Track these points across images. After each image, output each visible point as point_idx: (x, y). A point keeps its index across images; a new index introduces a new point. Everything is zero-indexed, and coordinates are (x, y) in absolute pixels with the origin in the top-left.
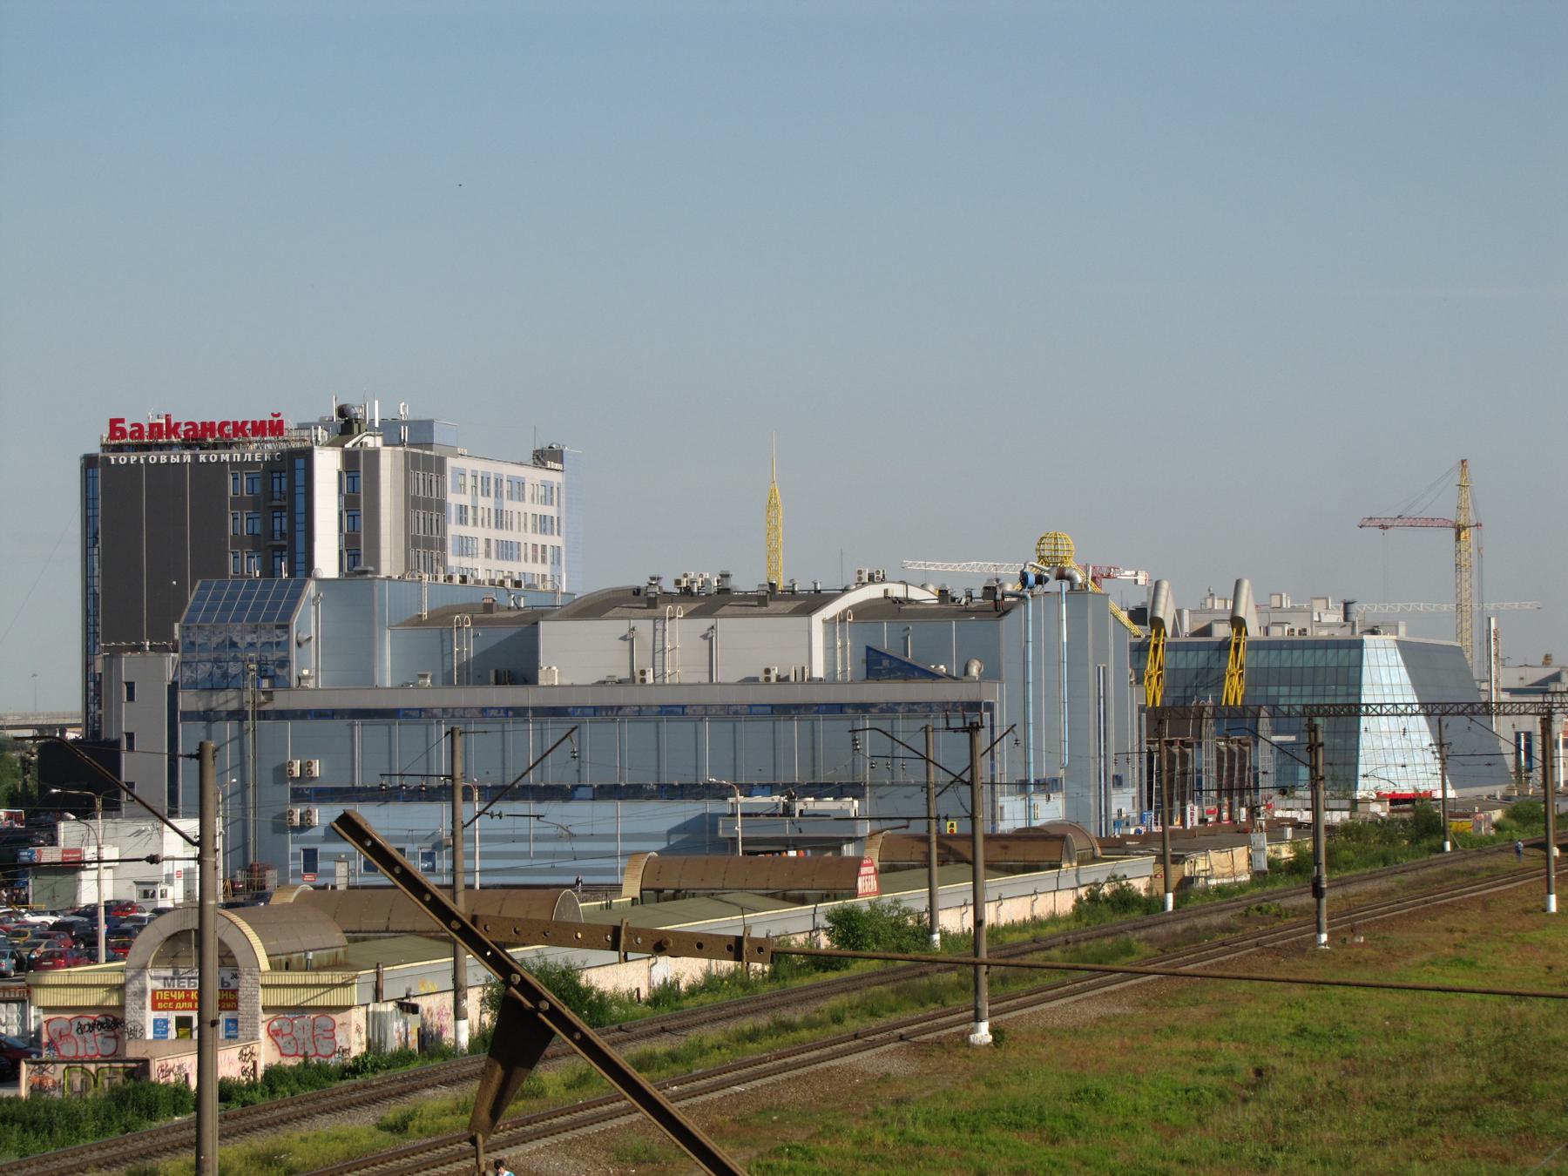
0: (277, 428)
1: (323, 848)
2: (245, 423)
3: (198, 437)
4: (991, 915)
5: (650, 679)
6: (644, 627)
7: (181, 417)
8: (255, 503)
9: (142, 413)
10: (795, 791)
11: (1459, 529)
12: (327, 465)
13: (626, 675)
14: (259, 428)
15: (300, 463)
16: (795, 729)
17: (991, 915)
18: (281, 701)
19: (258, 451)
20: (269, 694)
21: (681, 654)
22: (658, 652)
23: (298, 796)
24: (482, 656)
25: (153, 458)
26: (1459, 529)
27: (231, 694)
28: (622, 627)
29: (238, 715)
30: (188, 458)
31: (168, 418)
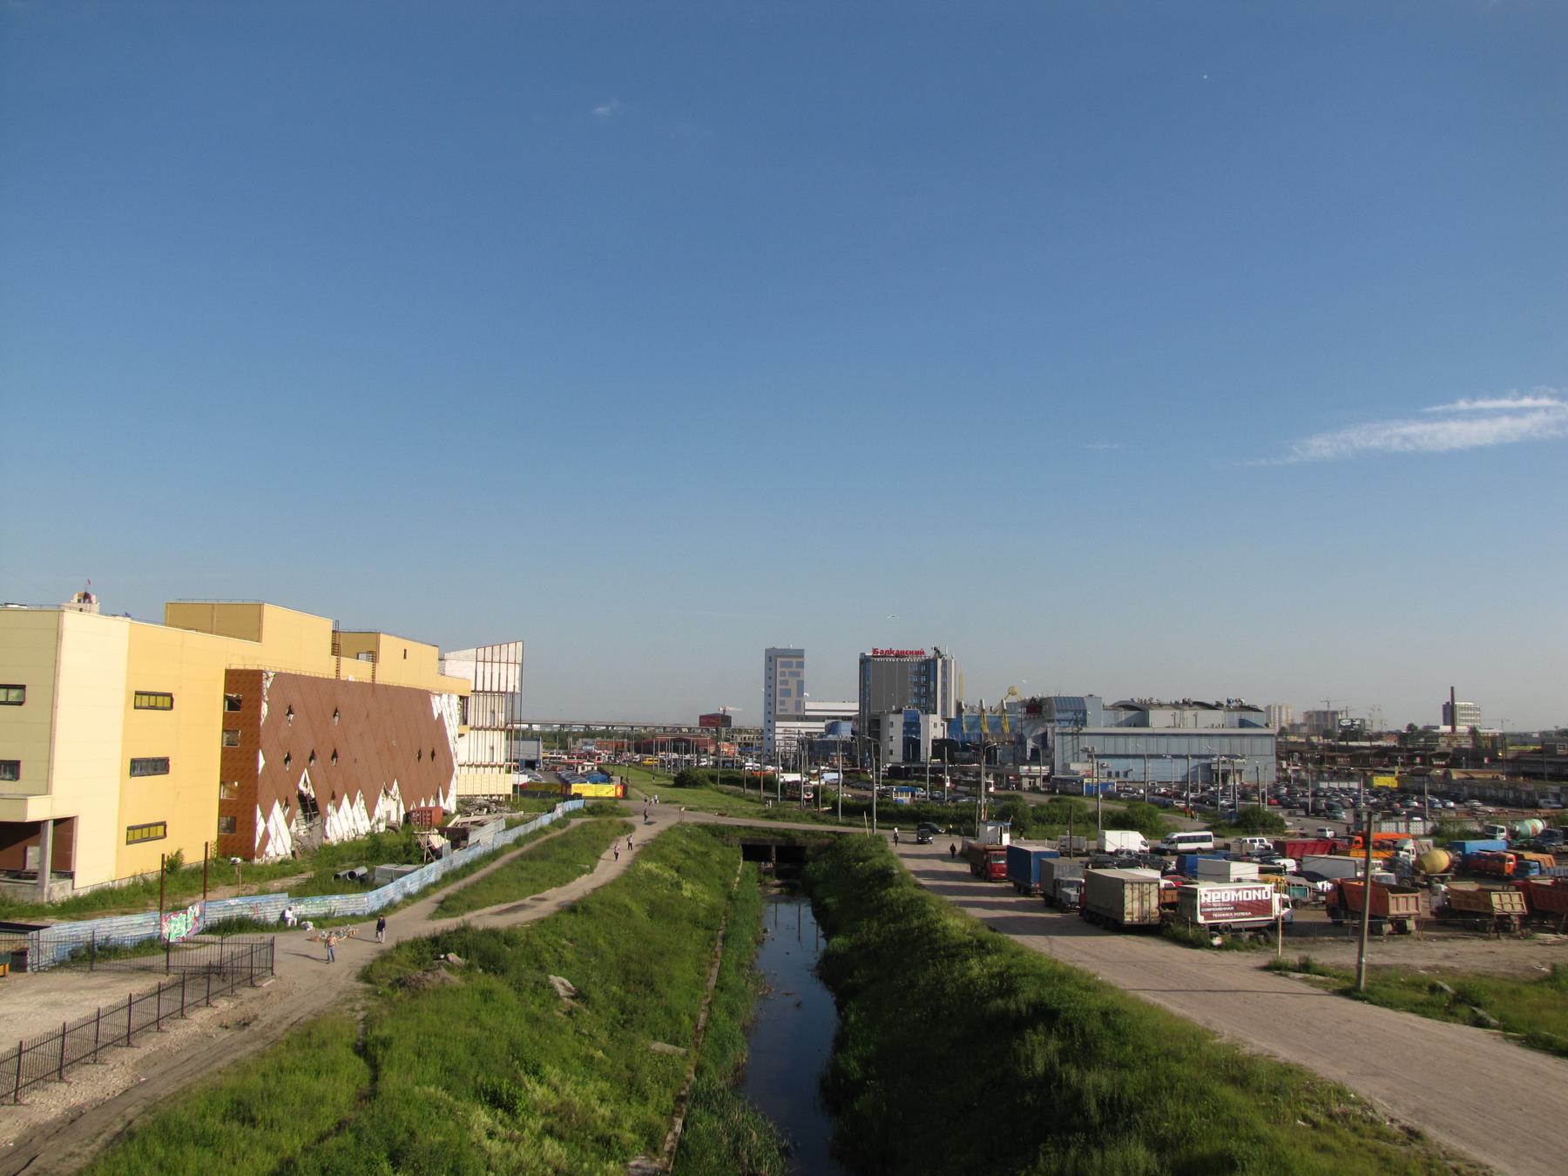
3: (900, 655)
7: (895, 649)
12: (940, 662)
18: (1085, 730)
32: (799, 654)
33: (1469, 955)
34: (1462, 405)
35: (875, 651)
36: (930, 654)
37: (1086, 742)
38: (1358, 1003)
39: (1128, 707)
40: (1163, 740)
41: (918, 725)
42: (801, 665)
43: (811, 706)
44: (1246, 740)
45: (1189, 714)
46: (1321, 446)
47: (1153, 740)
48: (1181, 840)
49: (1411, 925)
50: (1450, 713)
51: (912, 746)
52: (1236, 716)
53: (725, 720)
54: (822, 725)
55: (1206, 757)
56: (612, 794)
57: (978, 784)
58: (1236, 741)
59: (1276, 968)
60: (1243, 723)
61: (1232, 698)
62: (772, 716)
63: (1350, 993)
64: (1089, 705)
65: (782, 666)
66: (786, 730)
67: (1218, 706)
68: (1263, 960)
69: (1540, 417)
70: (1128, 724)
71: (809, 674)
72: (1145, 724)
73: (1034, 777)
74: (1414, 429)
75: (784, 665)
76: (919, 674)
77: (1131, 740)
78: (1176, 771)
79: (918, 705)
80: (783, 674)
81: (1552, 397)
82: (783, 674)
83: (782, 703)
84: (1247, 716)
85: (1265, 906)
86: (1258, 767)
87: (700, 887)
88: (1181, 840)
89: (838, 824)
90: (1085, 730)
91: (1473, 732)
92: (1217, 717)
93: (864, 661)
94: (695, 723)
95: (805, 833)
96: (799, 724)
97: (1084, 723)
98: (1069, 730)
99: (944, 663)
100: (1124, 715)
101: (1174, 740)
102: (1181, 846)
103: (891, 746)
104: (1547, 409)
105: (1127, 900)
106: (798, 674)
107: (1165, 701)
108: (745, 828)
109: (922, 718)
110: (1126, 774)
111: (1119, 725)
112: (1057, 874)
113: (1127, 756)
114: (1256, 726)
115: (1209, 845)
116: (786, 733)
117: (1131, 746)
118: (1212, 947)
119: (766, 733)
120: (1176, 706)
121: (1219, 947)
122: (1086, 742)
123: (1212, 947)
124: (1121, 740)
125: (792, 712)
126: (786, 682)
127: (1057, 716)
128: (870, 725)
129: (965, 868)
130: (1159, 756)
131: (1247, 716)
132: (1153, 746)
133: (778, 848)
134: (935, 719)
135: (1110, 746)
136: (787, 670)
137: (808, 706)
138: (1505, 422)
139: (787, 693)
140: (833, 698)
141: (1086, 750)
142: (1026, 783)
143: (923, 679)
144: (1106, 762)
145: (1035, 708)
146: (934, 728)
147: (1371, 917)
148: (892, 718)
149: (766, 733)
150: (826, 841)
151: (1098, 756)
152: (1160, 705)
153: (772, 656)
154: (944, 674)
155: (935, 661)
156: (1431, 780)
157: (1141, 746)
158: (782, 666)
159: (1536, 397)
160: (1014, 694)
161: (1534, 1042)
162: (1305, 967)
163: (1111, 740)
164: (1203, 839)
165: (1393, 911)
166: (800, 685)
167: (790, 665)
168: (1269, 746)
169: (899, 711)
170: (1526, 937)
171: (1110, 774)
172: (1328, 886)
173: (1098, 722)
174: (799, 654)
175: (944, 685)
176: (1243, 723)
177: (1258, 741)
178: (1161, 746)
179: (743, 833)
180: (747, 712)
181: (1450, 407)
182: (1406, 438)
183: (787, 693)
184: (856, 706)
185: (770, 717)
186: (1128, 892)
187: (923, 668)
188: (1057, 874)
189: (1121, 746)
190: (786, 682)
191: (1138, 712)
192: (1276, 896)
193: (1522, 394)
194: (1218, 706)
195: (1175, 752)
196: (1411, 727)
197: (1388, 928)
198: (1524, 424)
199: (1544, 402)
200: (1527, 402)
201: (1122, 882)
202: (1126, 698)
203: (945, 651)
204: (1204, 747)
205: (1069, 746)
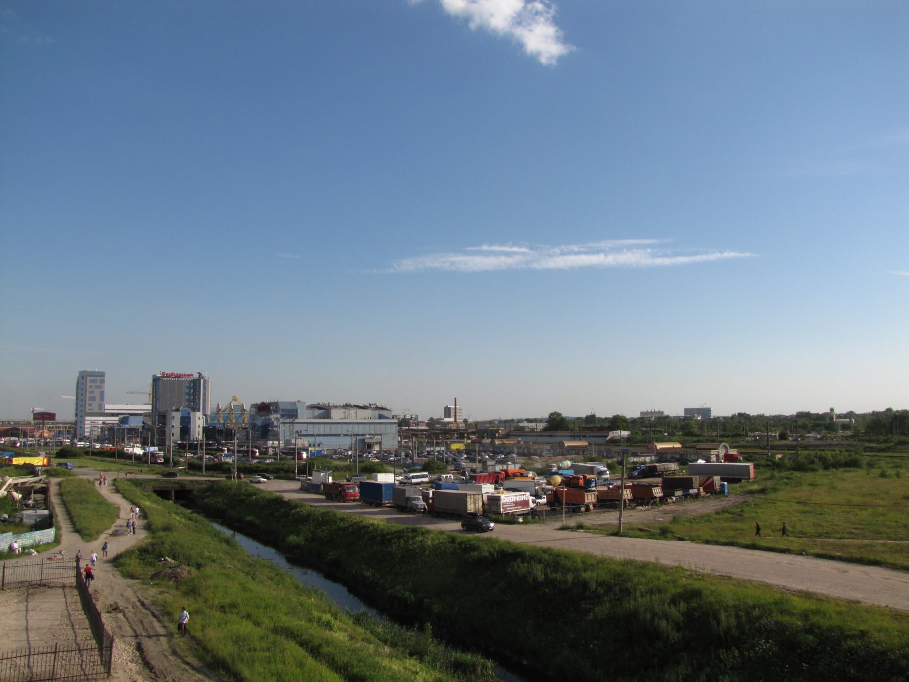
7: (175, 373)
12: (202, 381)
16: (372, 426)
18: (297, 421)
19: (190, 379)
22: (349, 414)
31: (832, 410)
32: (102, 375)
33: (610, 518)
34: (485, 248)
36: (196, 376)
37: (297, 428)
38: (624, 538)
39: (318, 407)
40: (339, 426)
41: (189, 418)
42: (103, 381)
43: (109, 407)
44: (383, 426)
45: (353, 411)
46: (408, 264)
47: (333, 426)
48: (413, 477)
49: (591, 507)
50: (447, 412)
51: (185, 430)
52: (377, 412)
53: (51, 416)
54: (117, 418)
55: (362, 435)
56: (41, 463)
57: (248, 452)
58: (378, 426)
59: (563, 528)
62: (81, 411)
63: (617, 534)
64: (299, 406)
65: (88, 385)
66: (92, 422)
67: (364, 408)
68: (558, 525)
69: (518, 258)
71: (108, 387)
72: (328, 416)
74: (459, 259)
75: (91, 381)
76: (189, 388)
77: (322, 426)
79: (189, 406)
80: (91, 387)
81: (527, 247)
82: (91, 387)
83: (90, 405)
85: (525, 503)
88: (413, 477)
89: (204, 476)
90: (297, 421)
91: (465, 421)
92: (368, 413)
93: (156, 380)
94: (31, 418)
95: (192, 481)
97: (296, 417)
98: (288, 421)
99: (205, 381)
100: (317, 412)
102: (414, 481)
103: (173, 431)
104: (523, 254)
105: (468, 504)
106: (100, 387)
107: (352, 404)
108: (154, 480)
109: (192, 414)
110: (319, 445)
111: (315, 418)
112: (407, 494)
113: (318, 435)
114: (388, 418)
115: (426, 480)
116: (92, 424)
117: (322, 429)
118: (519, 523)
121: (522, 523)
122: (297, 428)
123: (519, 523)
124: (316, 426)
125: (96, 410)
126: (92, 392)
128: (160, 417)
129: (323, 497)
130: (339, 435)
133: (176, 491)
134: (199, 414)
136: (94, 385)
137: (107, 407)
138: (503, 259)
139: (93, 399)
141: (297, 432)
143: (192, 391)
145: (264, 408)
146: (198, 423)
147: (567, 504)
148: (174, 414)
150: (205, 486)
152: (336, 407)
154: (205, 388)
155: (199, 380)
156: (484, 445)
157: (327, 429)
158: (88, 385)
159: (520, 247)
160: (236, 400)
161: (707, 542)
162: (580, 527)
164: (423, 476)
165: (586, 501)
166: (102, 395)
167: (95, 381)
168: (395, 428)
169: (177, 410)
170: (633, 509)
173: (304, 416)
174: (102, 375)
175: (204, 394)
176: (381, 417)
177: (389, 426)
178: (338, 429)
179: (153, 483)
180: (66, 414)
181: (479, 248)
182: (453, 263)
183: (93, 399)
184: (150, 407)
186: (469, 500)
187: (192, 384)
188: (407, 494)
190: (92, 392)
191: (325, 411)
192: (531, 498)
193: (514, 245)
194: (364, 408)
196: (431, 419)
197: (583, 509)
198: (510, 261)
199: (523, 250)
200: (515, 249)
201: (466, 495)
202: (315, 403)
204: (360, 430)
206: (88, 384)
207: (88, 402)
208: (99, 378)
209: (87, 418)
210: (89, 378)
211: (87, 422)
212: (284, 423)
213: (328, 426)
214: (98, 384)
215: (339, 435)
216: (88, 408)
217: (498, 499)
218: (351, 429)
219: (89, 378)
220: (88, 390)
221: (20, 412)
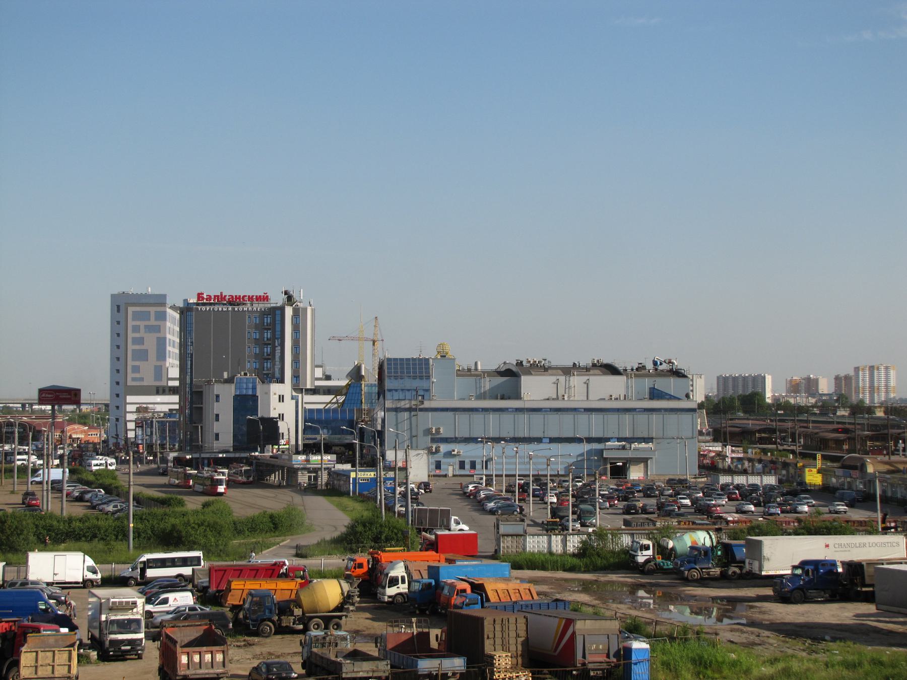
0: (265, 298)
1: (443, 461)
2: (244, 296)
3: (234, 301)
4: (319, 458)
5: (566, 398)
6: (562, 379)
7: (227, 293)
8: (256, 327)
9: (210, 290)
10: (630, 440)
11: (374, 342)
12: (289, 311)
13: (555, 397)
14: (259, 298)
15: (278, 312)
16: (627, 417)
17: (319, 458)
18: (427, 404)
19: (259, 306)
20: (422, 403)
21: (577, 390)
22: (568, 388)
23: (433, 440)
24: (491, 389)
25: (216, 308)
26: (374, 342)
27: (407, 402)
28: (554, 378)
29: (410, 410)
30: (230, 309)
31: (221, 293)
35: (200, 296)
36: (277, 299)
37: (429, 421)
40: (537, 418)
41: (254, 398)
44: (654, 417)
47: (524, 418)
52: (647, 383)
53: (71, 396)
60: (655, 394)
61: (659, 358)
62: (121, 387)
70: (495, 395)
72: (516, 395)
73: (316, 471)
75: (137, 316)
76: (261, 327)
78: (559, 458)
80: (136, 329)
82: (136, 329)
83: (136, 369)
84: (662, 384)
86: (672, 455)
87: (488, 644)
92: (614, 386)
96: (159, 399)
98: (405, 404)
99: (296, 313)
101: (553, 418)
103: (217, 427)
107: (557, 361)
110: (486, 464)
111: (481, 396)
114: (672, 398)
119: (110, 413)
120: (567, 371)
124: (478, 418)
125: (149, 381)
126: (140, 341)
127: (861, 396)
131: (662, 384)
132: (525, 426)
135: (463, 426)
136: (142, 324)
139: (142, 355)
140: (825, 387)
141: (428, 432)
142: (303, 479)
144: (457, 448)
148: (218, 389)
149: (110, 413)
151: (446, 440)
153: (121, 305)
154: (296, 328)
155: (282, 309)
157: (507, 426)
163: (463, 418)
167: (145, 316)
171: (462, 465)
172: (183, 599)
173: (445, 392)
176: (655, 394)
177: (673, 417)
183: (142, 355)
185: (120, 389)
189: (478, 426)
190: (140, 341)
195: (555, 435)
202: (606, 361)
203: (300, 296)
204: (594, 426)
205: (406, 425)
206: (131, 323)
207: (130, 363)
208: (152, 310)
209: (130, 399)
210: (131, 310)
211: (130, 408)
212: (396, 410)
213: (507, 418)
214: (153, 322)
215: (539, 440)
216: (130, 375)
217: (628, 651)
218: (564, 426)
219: (131, 310)
220: (131, 335)
221: (13, 386)
